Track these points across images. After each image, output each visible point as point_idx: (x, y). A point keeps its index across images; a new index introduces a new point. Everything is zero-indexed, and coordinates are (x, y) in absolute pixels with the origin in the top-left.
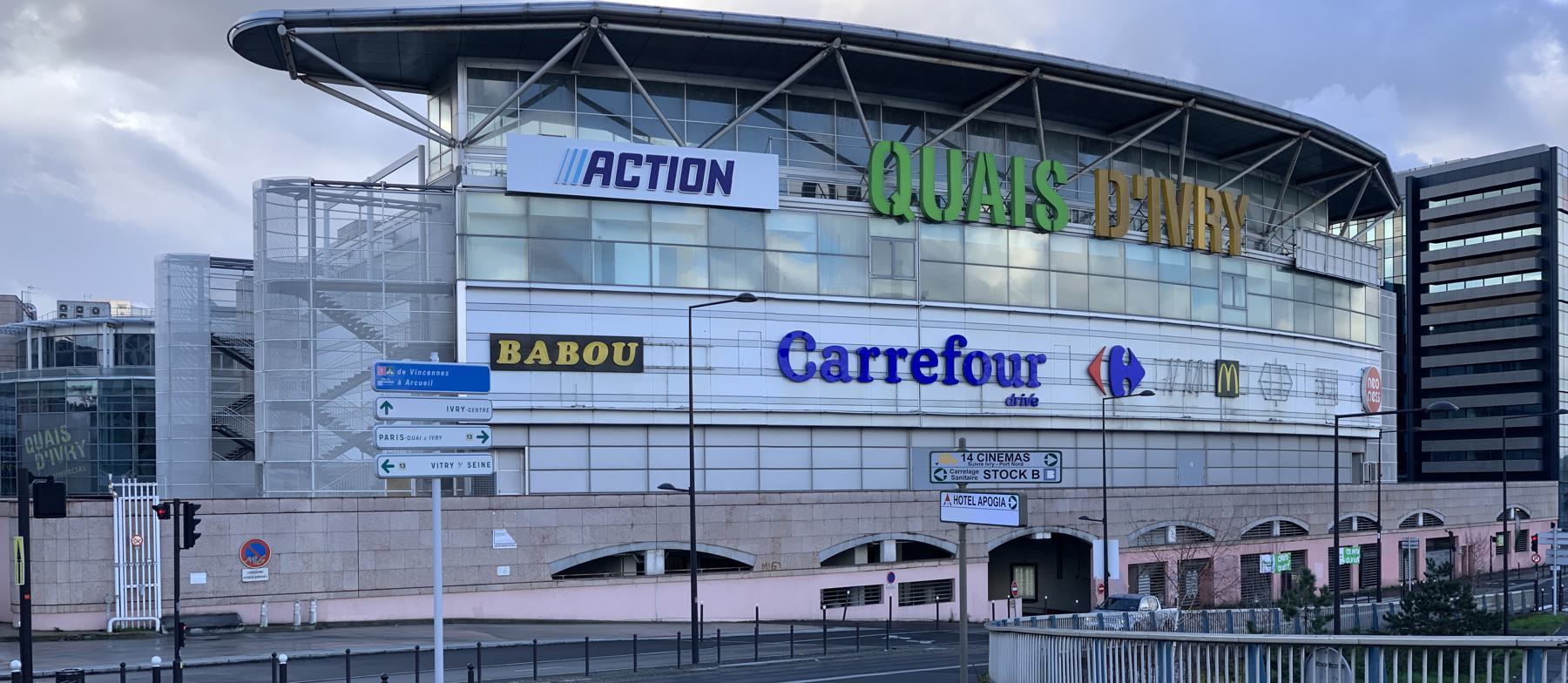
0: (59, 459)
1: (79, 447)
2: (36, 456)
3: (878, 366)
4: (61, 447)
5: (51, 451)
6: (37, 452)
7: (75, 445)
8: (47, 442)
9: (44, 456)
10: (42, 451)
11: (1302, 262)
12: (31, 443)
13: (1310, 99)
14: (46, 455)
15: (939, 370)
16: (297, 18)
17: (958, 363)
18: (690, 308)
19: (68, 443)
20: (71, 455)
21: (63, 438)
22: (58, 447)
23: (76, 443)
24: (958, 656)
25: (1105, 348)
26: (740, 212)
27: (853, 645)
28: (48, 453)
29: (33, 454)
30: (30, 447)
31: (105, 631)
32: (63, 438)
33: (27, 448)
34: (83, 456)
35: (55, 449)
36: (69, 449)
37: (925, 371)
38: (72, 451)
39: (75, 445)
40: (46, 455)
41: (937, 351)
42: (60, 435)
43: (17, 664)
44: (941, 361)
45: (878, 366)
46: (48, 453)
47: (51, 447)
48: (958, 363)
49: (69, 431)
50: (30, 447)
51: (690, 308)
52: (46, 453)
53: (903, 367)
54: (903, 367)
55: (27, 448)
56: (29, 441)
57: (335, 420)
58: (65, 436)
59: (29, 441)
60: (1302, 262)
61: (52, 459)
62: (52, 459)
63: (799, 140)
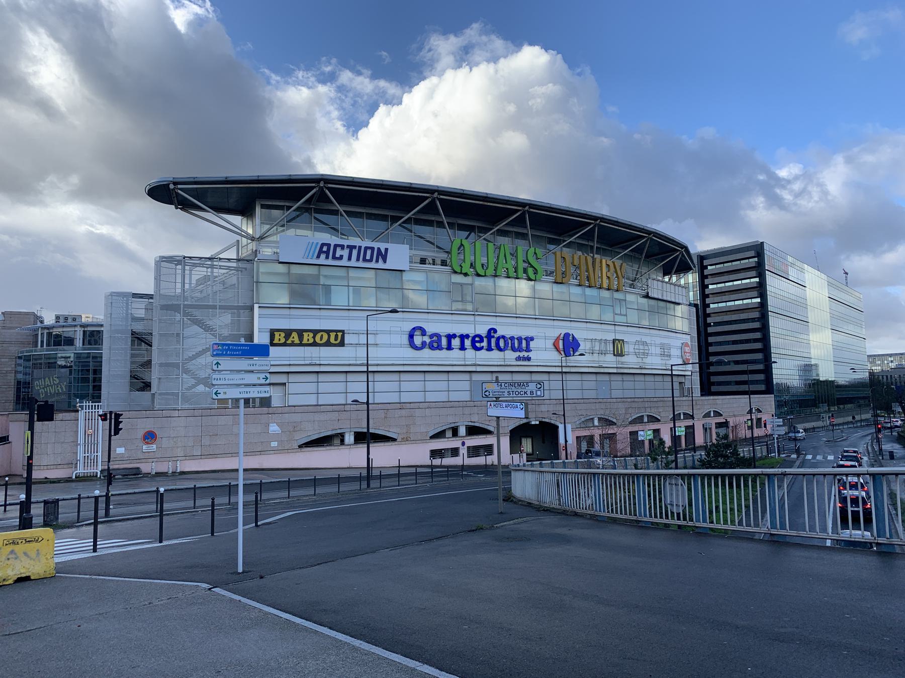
3: (456, 342)
4: (53, 386)
6: (41, 388)
12: (38, 384)
15: (485, 344)
17: (493, 341)
29: (39, 390)
36: (57, 387)
37: (478, 345)
44: (485, 340)
45: (456, 342)
47: (48, 386)
48: (493, 341)
52: (45, 389)
53: (468, 343)
54: (468, 343)
56: (37, 384)
58: (55, 380)
59: (37, 384)
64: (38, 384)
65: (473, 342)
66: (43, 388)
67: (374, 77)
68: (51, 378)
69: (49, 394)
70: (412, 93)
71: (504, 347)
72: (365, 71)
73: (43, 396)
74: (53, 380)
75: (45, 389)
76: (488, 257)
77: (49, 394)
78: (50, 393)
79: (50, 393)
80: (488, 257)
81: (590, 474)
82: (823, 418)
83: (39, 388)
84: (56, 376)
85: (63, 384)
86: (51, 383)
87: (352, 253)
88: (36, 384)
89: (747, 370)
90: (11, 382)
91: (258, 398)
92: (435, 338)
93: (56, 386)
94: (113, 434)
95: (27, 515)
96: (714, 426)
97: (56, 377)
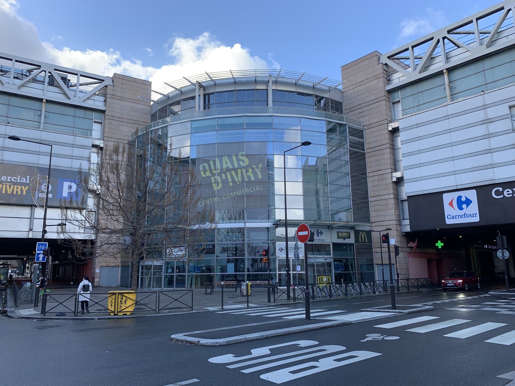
0: (237, 180)
1: (256, 170)
2: (212, 178)
3: (457, 217)
4: (239, 171)
5: (228, 174)
6: (214, 175)
7: (253, 168)
8: (225, 166)
9: (221, 178)
12: (207, 168)
14: (224, 178)
15: (464, 216)
17: (466, 216)
19: (247, 166)
20: (249, 177)
21: (241, 163)
22: (236, 170)
23: (254, 167)
24: (270, 302)
25: (184, 335)
27: (378, 278)
30: (205, 171)
31: (273, 284)
32: (241, 163)
33: (202, 173)
34: (260, 177)
35: (233, 172)
36: (247, 171)
37: (462, 217)
38: (250, 173)
39: (253, 168)
40: (224, 178)
41: (463, 215)
43: (382, 267)
44: (464, 216)
45: (457, 217)
46: (226, 176)
47: (228, 170)
48: (466, 216)
49: (247, 156)
50: (205, 171)
52: (223, 175)
53: (460, 217)
54: (460, 217)
55: (202, 173)
58: (243, 161)
61: (230, 180)
62: (230, 180)
64: (207, 168)
65: (461, 216)
66: (220, 174)
68: (234, 158)
69: (231, 184)
73: (219, 188)
74: (238, 160)
77: (231, 184)
78: (234, 181)
79: (234, 181)
81: (47, 228)
82: (83, 254)
83: (208, 174)
84: (244, 153)
85: (258, 168)
86: (242, 171)
87: (460, 189)
88: (201, 168)
90: (106, 155)
92: (453, 216)
93: (244, 171)
95: (307, 291)
96: (213, 243)
97: (242, 155)
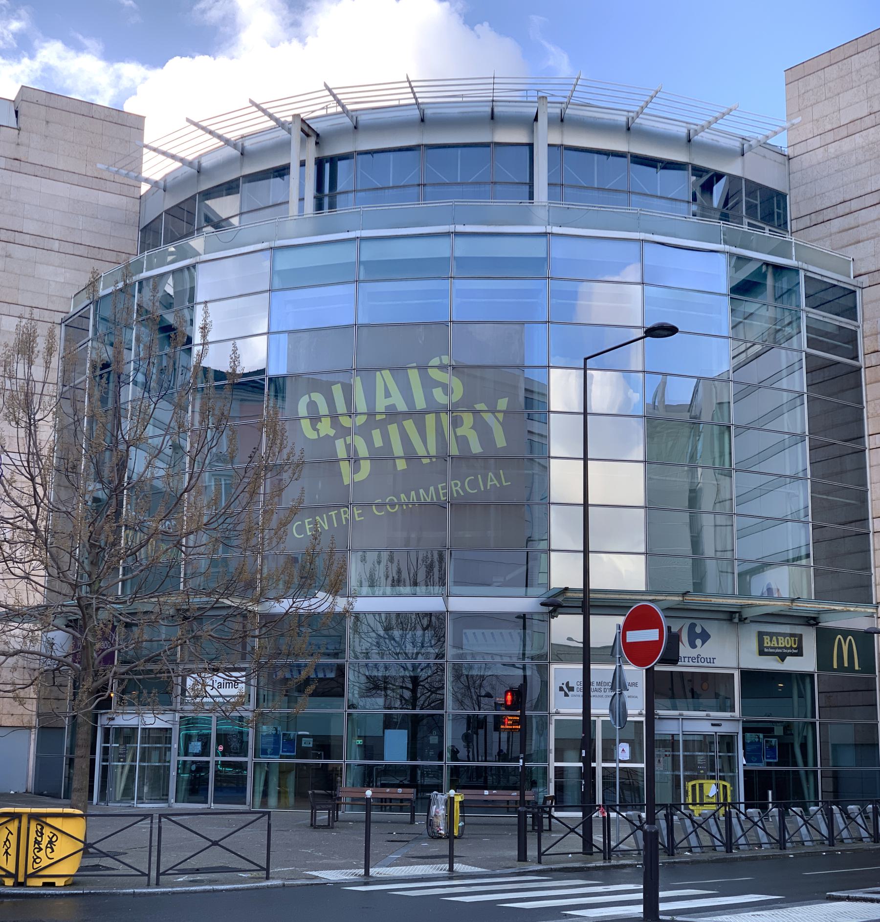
0: (421, 451)
1: (487, 417)
9: (369, 442)
10: (365, 431)
11: (642, 118)
12: (323, 409)
13: (162, 68)
14: (378, 442)
16: (576, 115)
18: (586, 359)
20: (462, 441)
26: (248, 255)
28: (386, 436)
29: (329, 440)
34: (501, 441)
36: (456, 423)
39: (476, 412)
40: (378, 442)
42: (428, 384)
46: (386, 436)
47: (392, 415)
51: (586, 359)
52: (376, 434)
55: (306, 424)
56: (312, 405)
57: (367, 674)
59: (312, 405)
60: (642, 118)
61: (398, 449)
63: (347, 190)
64: (323, 409)
67: (111, 55)
69: (401, 465)
70: (159, 72)
71: (289, 771)
72: (88, 42)
75: (376, 434)
76: (393, 187)
78: (411, 457)
79: (411, 457)
80: (393, 187)
83: (325, 428)
85: (493, 411)
88: (302, 410)
89: (447, 259)
91: (846, 633)
94: (809, 274)
